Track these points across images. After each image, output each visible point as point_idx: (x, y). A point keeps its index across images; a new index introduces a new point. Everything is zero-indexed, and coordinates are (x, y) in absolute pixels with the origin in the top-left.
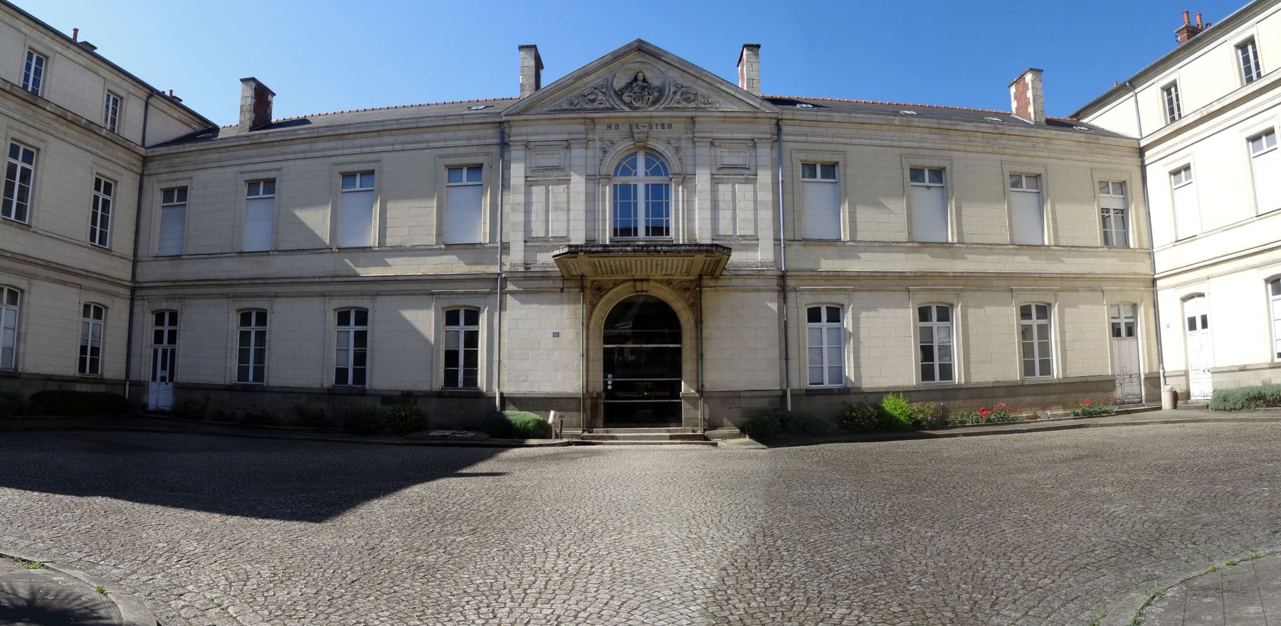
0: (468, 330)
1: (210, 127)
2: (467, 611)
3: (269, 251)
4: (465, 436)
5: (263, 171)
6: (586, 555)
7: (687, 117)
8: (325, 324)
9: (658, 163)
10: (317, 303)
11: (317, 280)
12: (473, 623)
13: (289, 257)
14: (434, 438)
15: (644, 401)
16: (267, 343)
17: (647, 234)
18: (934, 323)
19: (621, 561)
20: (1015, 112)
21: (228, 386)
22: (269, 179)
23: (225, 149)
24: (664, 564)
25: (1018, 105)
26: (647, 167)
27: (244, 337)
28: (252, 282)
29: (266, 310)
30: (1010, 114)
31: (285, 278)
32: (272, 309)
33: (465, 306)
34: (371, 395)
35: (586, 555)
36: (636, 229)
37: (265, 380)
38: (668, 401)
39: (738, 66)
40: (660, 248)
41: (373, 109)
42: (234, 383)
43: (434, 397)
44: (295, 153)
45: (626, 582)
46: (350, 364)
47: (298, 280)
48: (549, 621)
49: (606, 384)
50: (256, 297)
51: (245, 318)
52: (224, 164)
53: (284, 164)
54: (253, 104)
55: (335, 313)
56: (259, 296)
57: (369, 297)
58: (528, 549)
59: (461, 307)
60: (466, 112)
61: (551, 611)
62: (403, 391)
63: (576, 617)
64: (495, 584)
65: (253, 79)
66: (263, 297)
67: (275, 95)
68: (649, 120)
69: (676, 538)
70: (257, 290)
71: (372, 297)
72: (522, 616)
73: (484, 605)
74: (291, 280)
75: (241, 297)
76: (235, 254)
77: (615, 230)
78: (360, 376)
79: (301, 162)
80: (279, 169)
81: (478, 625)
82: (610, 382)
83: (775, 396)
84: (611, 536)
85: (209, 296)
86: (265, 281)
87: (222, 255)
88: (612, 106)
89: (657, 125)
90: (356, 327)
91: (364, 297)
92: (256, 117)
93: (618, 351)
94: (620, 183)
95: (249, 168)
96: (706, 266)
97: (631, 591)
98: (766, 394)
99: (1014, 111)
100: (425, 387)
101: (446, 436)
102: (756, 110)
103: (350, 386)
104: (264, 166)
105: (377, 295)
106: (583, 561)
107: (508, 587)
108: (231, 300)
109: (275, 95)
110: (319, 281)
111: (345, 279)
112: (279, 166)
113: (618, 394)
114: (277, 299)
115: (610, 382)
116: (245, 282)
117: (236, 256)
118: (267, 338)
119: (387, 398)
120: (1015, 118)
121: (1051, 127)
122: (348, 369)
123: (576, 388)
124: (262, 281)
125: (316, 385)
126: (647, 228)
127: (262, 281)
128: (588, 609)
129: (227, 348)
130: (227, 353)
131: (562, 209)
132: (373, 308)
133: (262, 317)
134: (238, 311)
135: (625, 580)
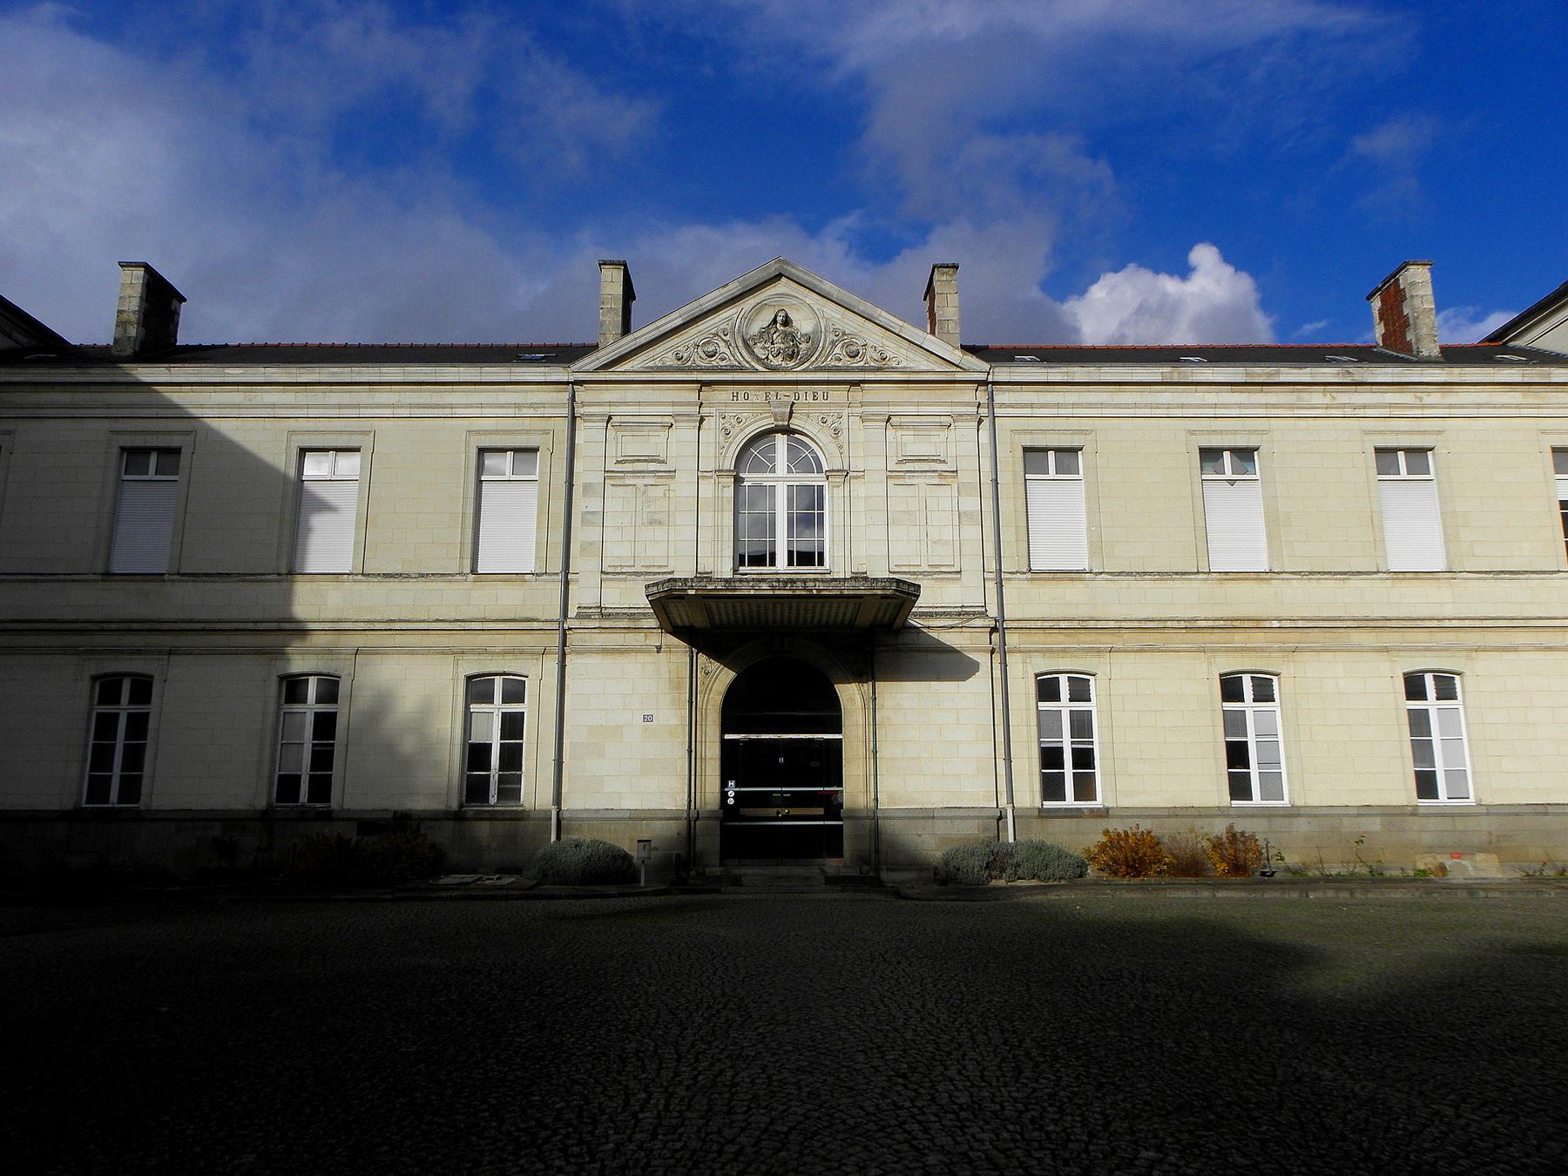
0: (488, 706)
2: (547, 1154)
3: (163, 574)
4: (499, 883)
6: (721, 1056)
11: (251, 626)
12: (560, 1170)
13: (200, 585)
14: (447, 888)
15: (826, 823)
16: (150, 735)
17: (790, 563)
18: (1248, 705)
19: (778, 1065)
24: (845, 1070)
27: (106, 725)
28: (128, 626)
34: (343, 820)
35: (721, 1056)
36: (773, 556)
37: (143, 799)
38: (822, 823)
40: (813, 584)
45: (791, 1097)
46: (304, 768)
48: (679, 1161)
49: (724, 796)
51: (108, 688)
52: (77, 413)
54: (142, 310)
56: (139, 652)
58: (630, 1050)
61: (681, 1144)
62: (395, 812)
63: (720, 1152)
64: (585, 1107)
65: (147, 268)
66: (146, 652)
67: (185, 300)
69: (857, 1030)
70: (137, 641)
72: (636, 1156)
73: (571, 1142)
74: (202, 625)
75: (102, 652)
76: (95, 577)
78: (321, 787)
81: (568, 1173)
82: (731, 794)
83: (989, 818)
84: (756, 1029)
85: (37, 651)
86: (153, 627)
87: (69, 578)
90: (317, 706)
93: (330, 751)
96: (881, 613)
97: (800, 1111)
98: (976, 813)
101: (468, 883)
102: (954, 369)
103: (303, 805)
105: (170, 653)
106: (717, 1068)
107: (607, 1111)
109: (185, 300)
113: (745, 811)
114: (174, 658)
115: (731, 794)
116: (113, 626)
117: (97, 581)
119: (368, 824)
122: (300, 776)
123: (679, 803)
125: (239, 805)
126: (790, 553)
127: (147, 626)
128: (739, 1139)
133: (143, 688)
135: (789, 1094)
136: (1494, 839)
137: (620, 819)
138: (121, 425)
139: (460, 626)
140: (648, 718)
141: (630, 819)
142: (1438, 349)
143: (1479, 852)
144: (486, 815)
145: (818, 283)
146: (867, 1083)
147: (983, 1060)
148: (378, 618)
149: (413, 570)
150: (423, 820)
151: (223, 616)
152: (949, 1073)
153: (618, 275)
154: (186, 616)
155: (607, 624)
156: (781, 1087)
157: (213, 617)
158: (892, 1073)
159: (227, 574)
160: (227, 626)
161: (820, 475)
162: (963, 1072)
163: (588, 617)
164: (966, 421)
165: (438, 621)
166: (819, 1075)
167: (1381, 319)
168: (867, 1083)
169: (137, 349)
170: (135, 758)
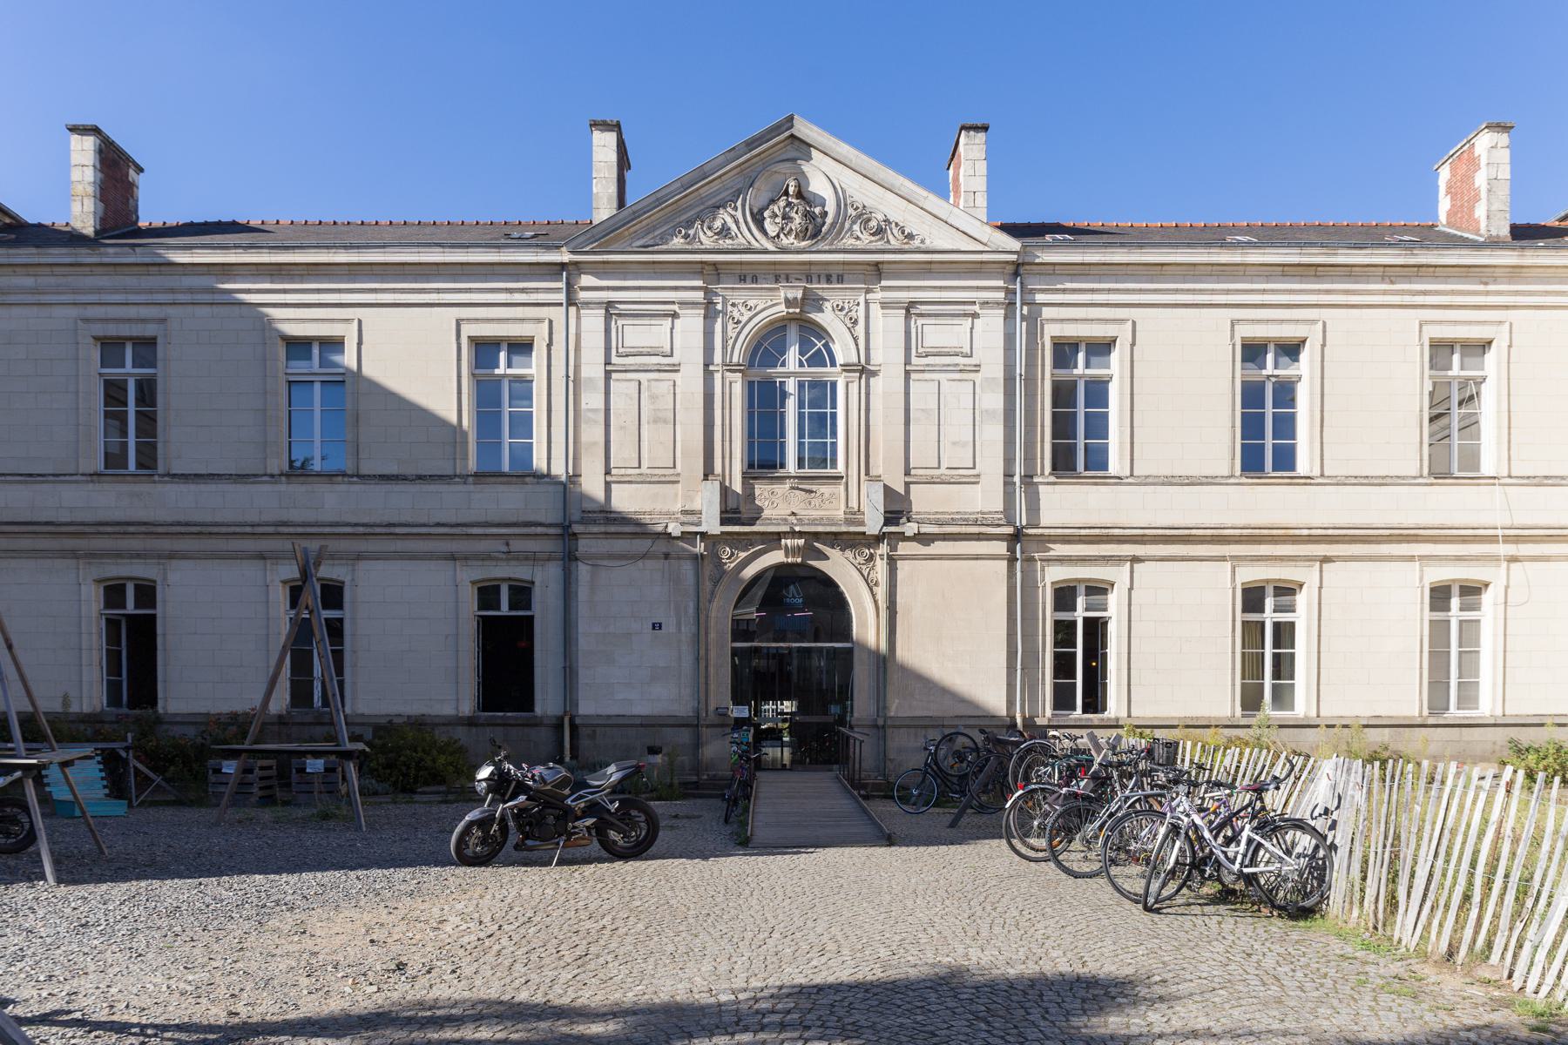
1: (8, 221)
5: (129, 320)
7: (868, 264)
8: (268, 607)
9: (819, 345)
10: (251, 570)
11: (248, 529)
13: (192, 487)
17: (801, 464)
20: (1444, 222)
21: (89, 715)
22: (144, 338)
23: (48, 269)
25: (1452, 206)
26: (802, 353)
28: (122, 528)
29: (155, 582)
30: (1433, 226)
31: (187, 524)
32: (165, 579)
33: (510, 579)
39: (948, 169)
41: (348, 223)
42: (98, 709)
43: (463, 725)
44: (191, 290)
47: (216, 530)
50: (132, 557)
53: (170, 311)
54: (98, 181)
55: (284, 587)
56: (138, 556)
57: (344, 562)
59: (504, 580)
60: (503, 241)
62: (409, 717)
65: (95, 131)
68: (808, 267)
71: (350, 562)
75: (102, 556)
76: (84, 478)
77: (751, 466)
79: (206, 310)
80: (163, 321)
89: (819, 276)
91: (336, 562)
92: (105, 213)
94: (759, 379)
95: (99, 312)
99: (1443, 218)
100: (448, 710)
104: (132, 312)
108: (81, 561)
109: (142, 170)
110: (253, 531)
111: (300, 530)
112: (162, 316)
114: (174, 562)
116: (109, 529)
118: (159, 630)
120: (1444, 232)
121: (1525, 243)
124: (143, 529)
127: (143, 529)
129: (81, 649)
130: (81, 658)
131: (665, 422)
132: (353, 580)
134: (99, 581)
136: (1497, 748)
137: (632, 726)
138: (92, 312)
139: (459, 529)
140: (657, 626)
141: (642, 725)
142: (1508, 229)
143: (1481, 761)
144: (499, 721)
145: (834, 146)
146: (948, 1028)
147: (1063, 1001)
148: (378, 521)
149: (410, 470)
150: (437, 725)
151: (218, 518)
152: (1031, 1017)
153: (610, 138)
154: (182, 518)
155: (612, 529)
156: (856, 1031)
157: (208, 518)
158: (972, 1017)
159: (218, 475)
160: (224, 530)
161: (833, 369)
162: (1047, 1016)
163: (594, 522)
164: (992, 308)
165: (438, 525)
166: (893, 1017)
167: (1448, 193)
168: (948, 1028)
169: (98, 227)
170: (148, 422)
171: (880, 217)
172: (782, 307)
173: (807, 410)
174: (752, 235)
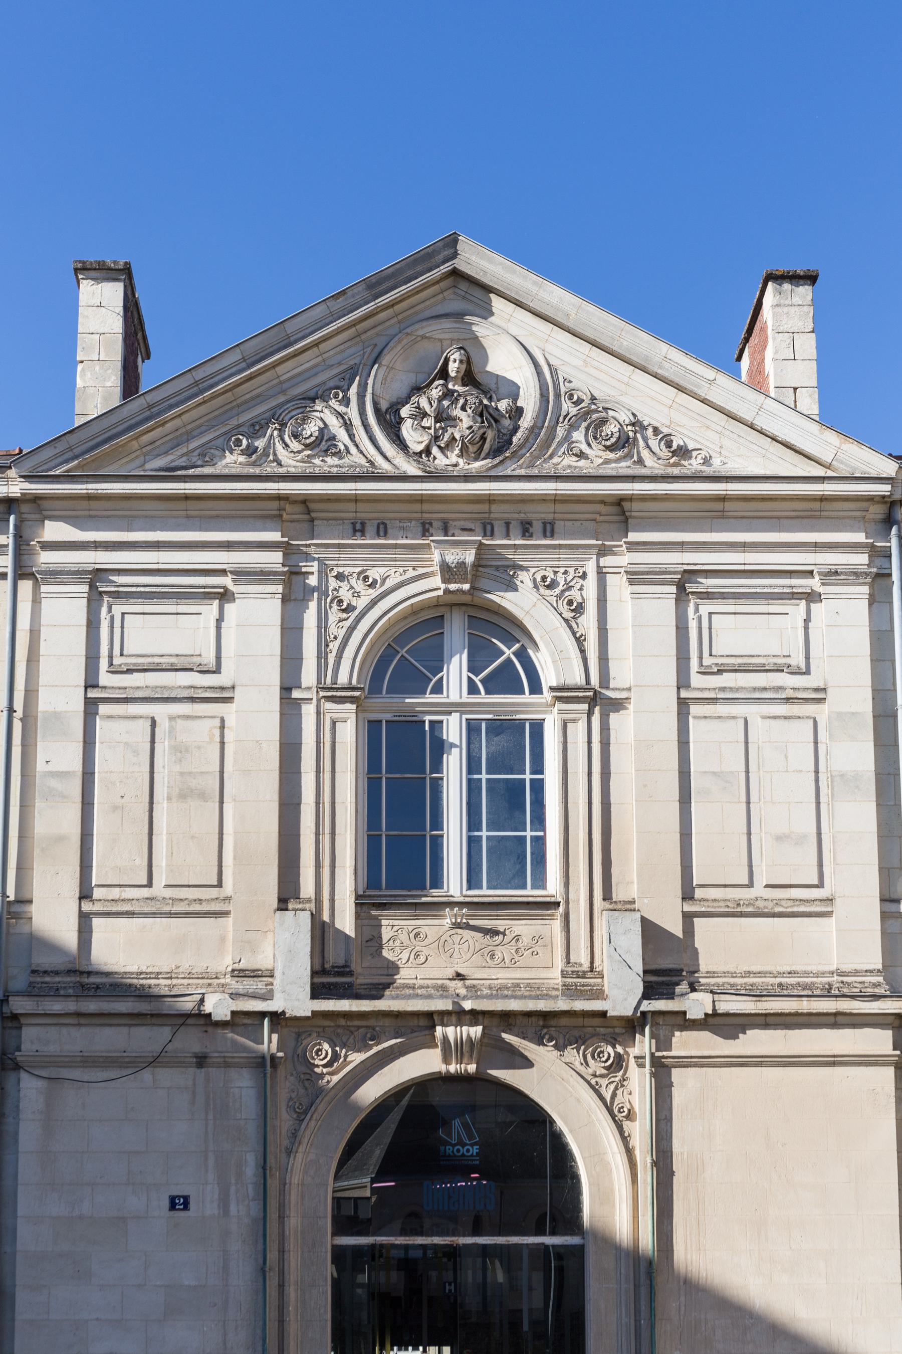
88: (371, 463)
161: (535, 698)
171: (625, 417)
172: (436, 581)
173: (484, 776)
174: (378, 448)
